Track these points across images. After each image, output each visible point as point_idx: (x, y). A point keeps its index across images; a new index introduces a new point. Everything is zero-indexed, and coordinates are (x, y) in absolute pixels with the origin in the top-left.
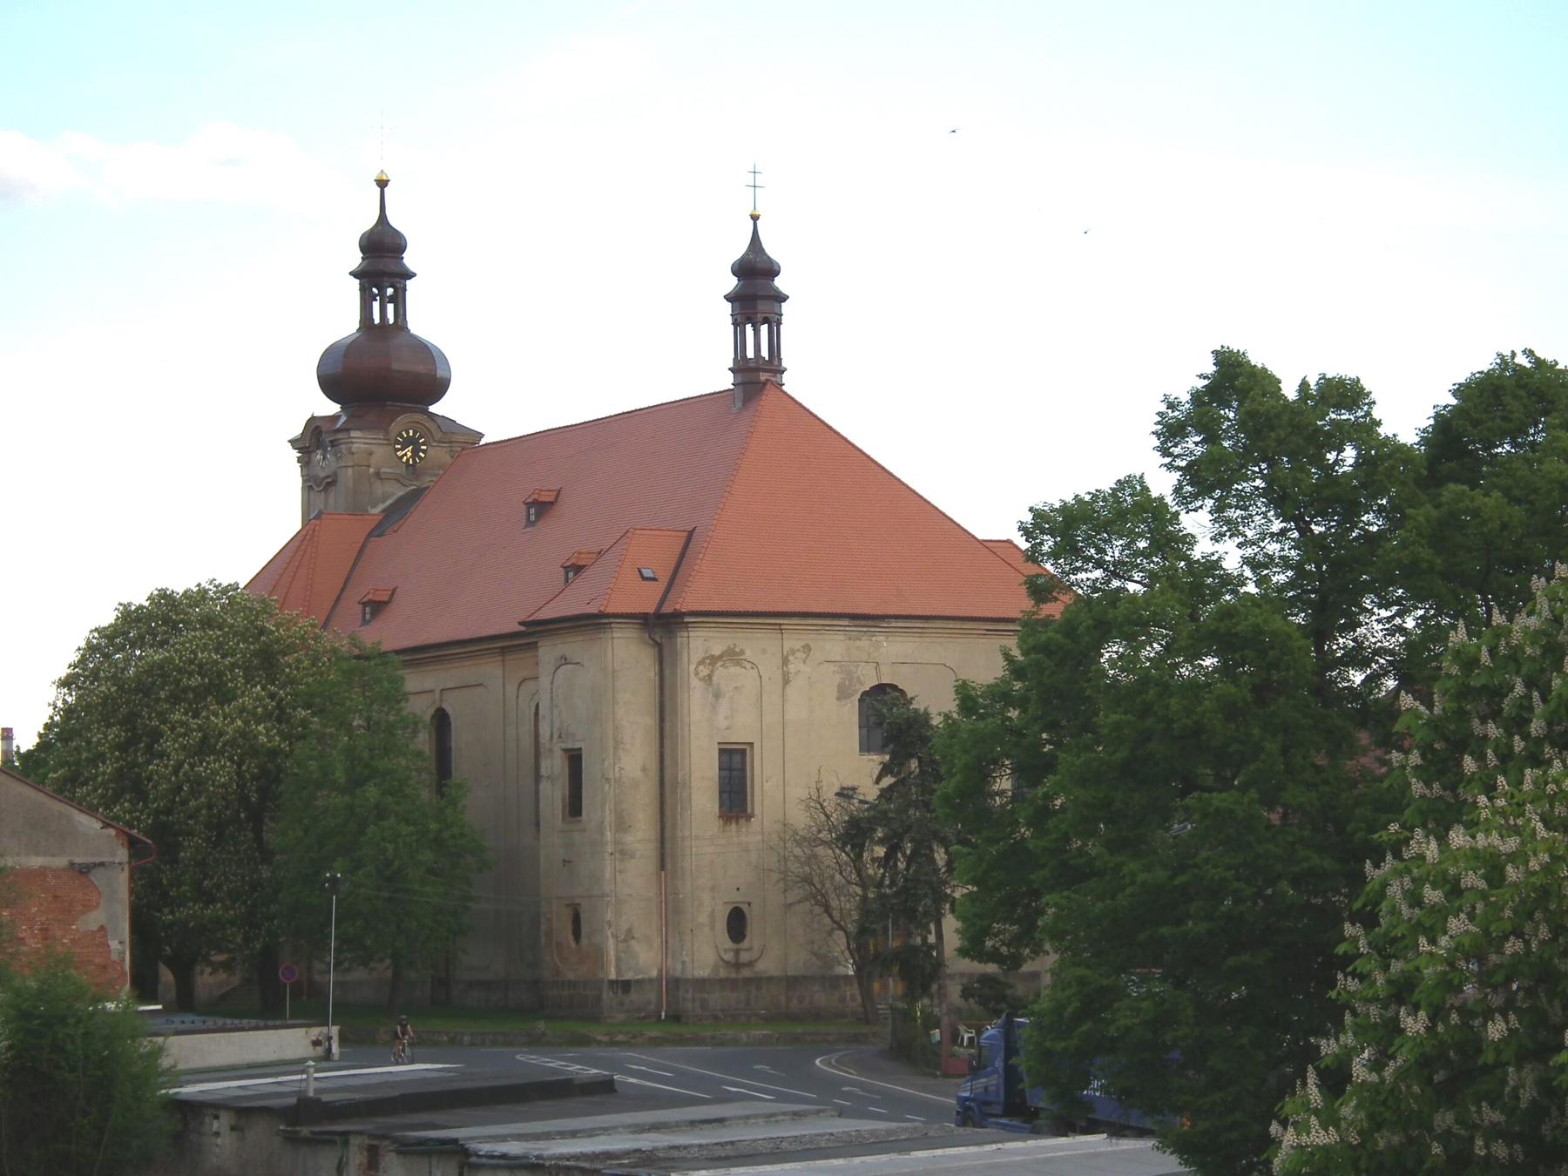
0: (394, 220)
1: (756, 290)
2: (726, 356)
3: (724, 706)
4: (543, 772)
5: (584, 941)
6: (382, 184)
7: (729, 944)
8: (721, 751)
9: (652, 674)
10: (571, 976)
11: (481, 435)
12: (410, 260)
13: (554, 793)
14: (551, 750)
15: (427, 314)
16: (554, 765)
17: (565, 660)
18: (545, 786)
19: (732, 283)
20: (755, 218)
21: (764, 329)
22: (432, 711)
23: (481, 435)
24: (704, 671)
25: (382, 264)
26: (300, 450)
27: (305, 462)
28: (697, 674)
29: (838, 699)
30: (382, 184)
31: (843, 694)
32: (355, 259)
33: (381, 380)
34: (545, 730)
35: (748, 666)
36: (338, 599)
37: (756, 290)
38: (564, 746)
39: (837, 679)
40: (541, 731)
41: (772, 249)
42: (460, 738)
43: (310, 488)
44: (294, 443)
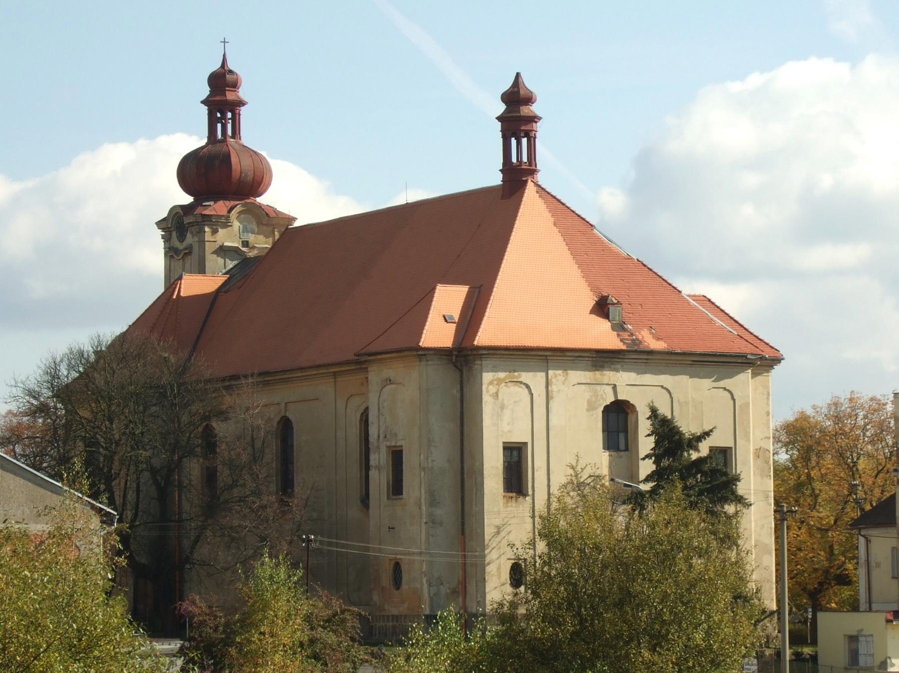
0: (231, 65)
1: (517, 116)
2: (498, 162)
3: (507, 412)
4: (372, 463)
5: (404, 586)
7: (509, 589)
8: (505, 448)
9: (455, 392)
10: (394, 611)
11: (294, 219)
12: (243, 93)
13: (379, 480)
14: (378, 447)
15: (255, 132)
16: (380, 458)
17: (389, 381)
18: (373, 474)
19: (501, 108)
21: (524, 141)
22: (277, 419)
23: (294, 219)
24: (492, 389)
25: (222, 96)
26: (163, 229)
27: (167, 239)
28: (487, 392)
29: (588, 410)
31: (591, 407)
32: (206, 91)
33: (217, 176)
34: (373, 431)
35: (524, 387)
36: (199, 337)
37: (517, 116)
38: (388, 444)
39: (587, 396)
40: (370, 432)
41: (530, 83)
42: (300, 438)
43: (172, 257)
44: (160, 224)
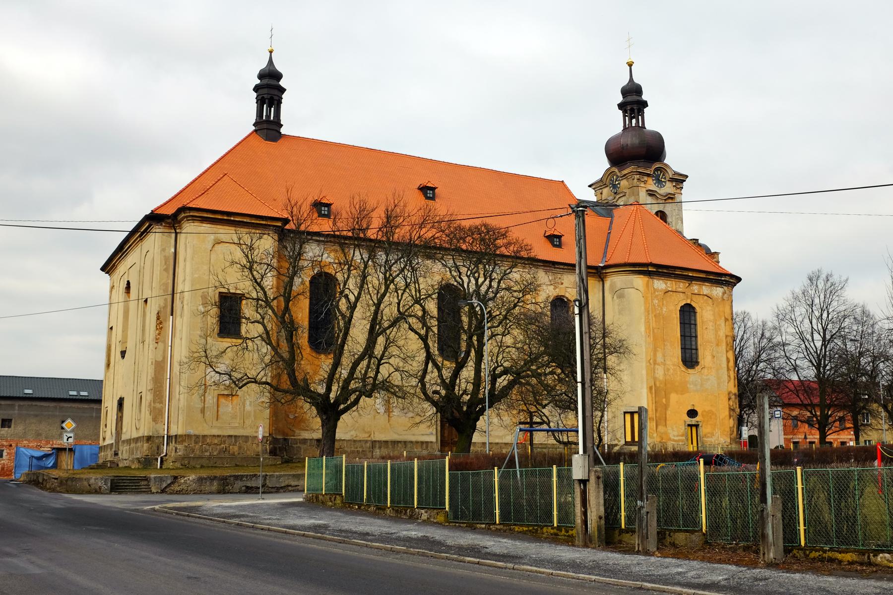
1: (270, 89)
6: (630, 65)
19: (282, 83)
20: (271, 52)
25: (633, 102)
30: (630, 65)
37: (270, 89)
41: (279, 67)
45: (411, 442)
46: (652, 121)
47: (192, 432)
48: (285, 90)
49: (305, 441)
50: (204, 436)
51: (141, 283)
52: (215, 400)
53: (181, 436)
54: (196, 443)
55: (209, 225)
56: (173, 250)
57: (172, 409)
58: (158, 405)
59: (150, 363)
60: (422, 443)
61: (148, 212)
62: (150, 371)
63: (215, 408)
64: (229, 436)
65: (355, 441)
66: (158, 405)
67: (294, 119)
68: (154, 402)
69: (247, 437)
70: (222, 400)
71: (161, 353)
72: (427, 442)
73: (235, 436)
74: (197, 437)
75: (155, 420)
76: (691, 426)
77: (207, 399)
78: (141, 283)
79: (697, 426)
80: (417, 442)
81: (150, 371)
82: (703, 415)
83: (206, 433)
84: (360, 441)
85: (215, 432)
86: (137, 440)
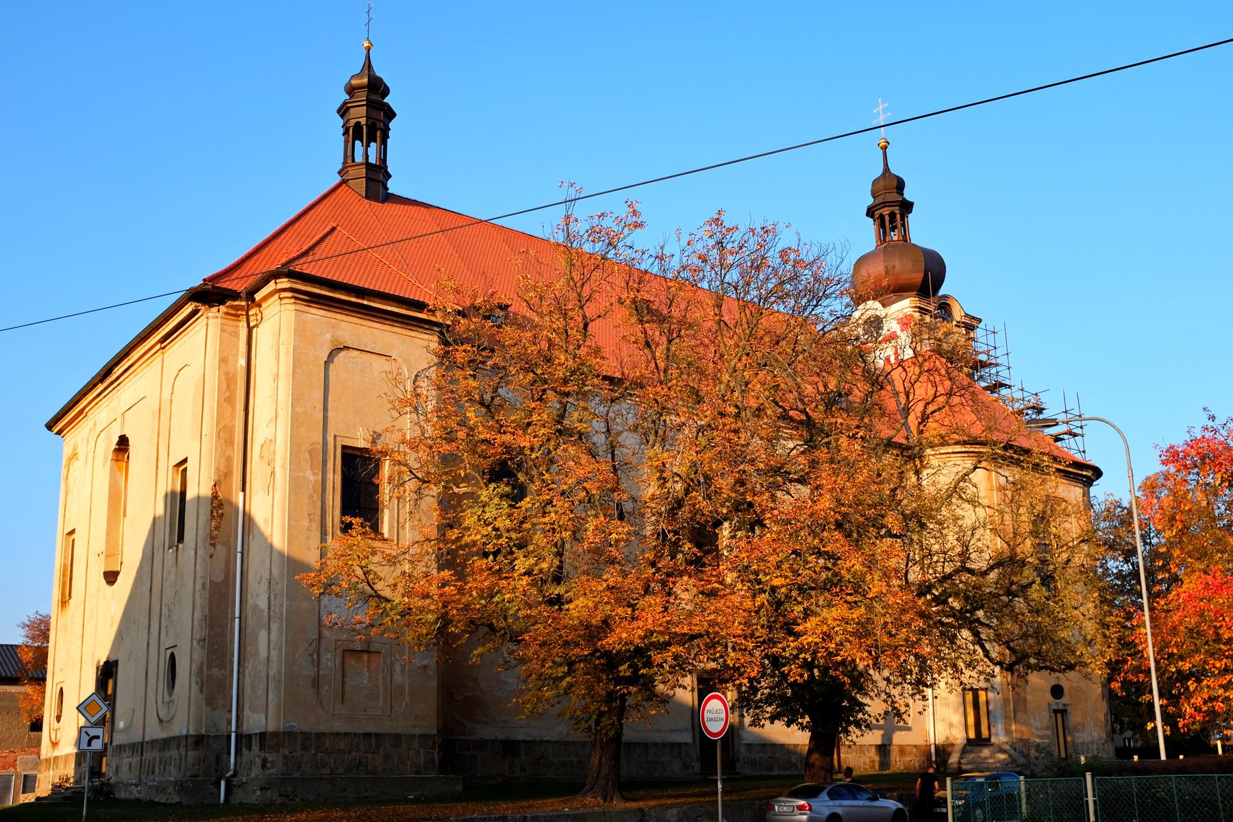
1: (370, 111)
37: (370, 111)
45: (656, 744)
46: (922, 230)
47: (298, 726)
48: (394, 115)
49: (482, 744)
50: (320, 735)
51: (162, 435)
52: (338, 661)
53: (275, 734)
54: (305, 748)
55: (321, 312)
56: (242, 362)
57: (248, 681)
58: (216, 672)
59: (199, 587)
60: (672, 745)
61: (196, 282)
62: (198, 602)
63: (339, 677)
64: (368, 735)
65: (566, 744)
66: (216, 672)
67: (416, 164)
68: (209, 667)
69: (398, 736)
70: (351, 662)
71: (222, 565)
72: (680, 745)
73: (377, 735)
74: (307, 736)
75: (210, 702)
76: (1056, 712)
77: (323, 660)
78: (162, 435)
79: (1063, 712)
80: (664, 744)
81: (198, 602)
82: (1070, 694)
83: (322, 728)
84: (575, 743)
85: (339, 726)
86: (166, 743)
